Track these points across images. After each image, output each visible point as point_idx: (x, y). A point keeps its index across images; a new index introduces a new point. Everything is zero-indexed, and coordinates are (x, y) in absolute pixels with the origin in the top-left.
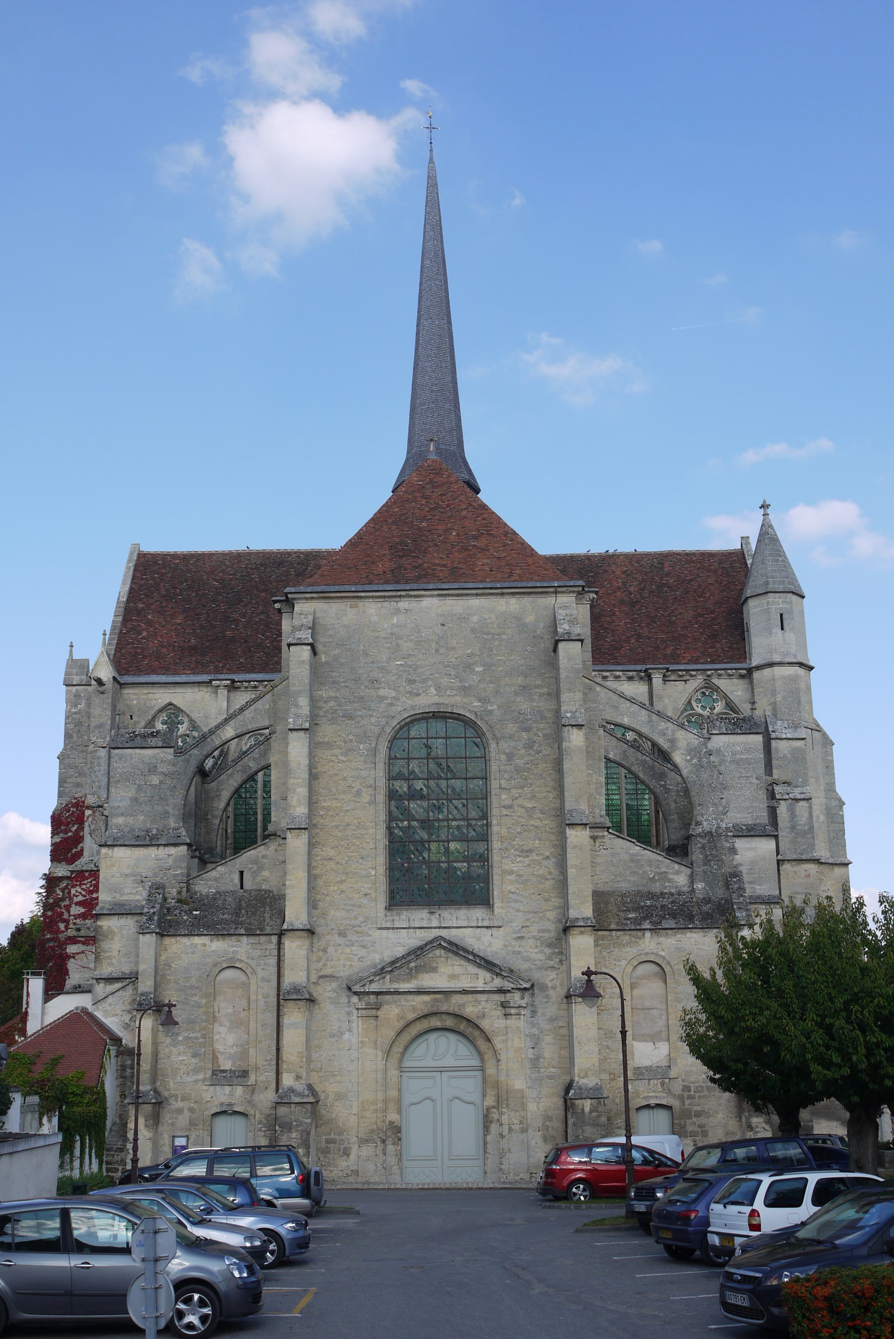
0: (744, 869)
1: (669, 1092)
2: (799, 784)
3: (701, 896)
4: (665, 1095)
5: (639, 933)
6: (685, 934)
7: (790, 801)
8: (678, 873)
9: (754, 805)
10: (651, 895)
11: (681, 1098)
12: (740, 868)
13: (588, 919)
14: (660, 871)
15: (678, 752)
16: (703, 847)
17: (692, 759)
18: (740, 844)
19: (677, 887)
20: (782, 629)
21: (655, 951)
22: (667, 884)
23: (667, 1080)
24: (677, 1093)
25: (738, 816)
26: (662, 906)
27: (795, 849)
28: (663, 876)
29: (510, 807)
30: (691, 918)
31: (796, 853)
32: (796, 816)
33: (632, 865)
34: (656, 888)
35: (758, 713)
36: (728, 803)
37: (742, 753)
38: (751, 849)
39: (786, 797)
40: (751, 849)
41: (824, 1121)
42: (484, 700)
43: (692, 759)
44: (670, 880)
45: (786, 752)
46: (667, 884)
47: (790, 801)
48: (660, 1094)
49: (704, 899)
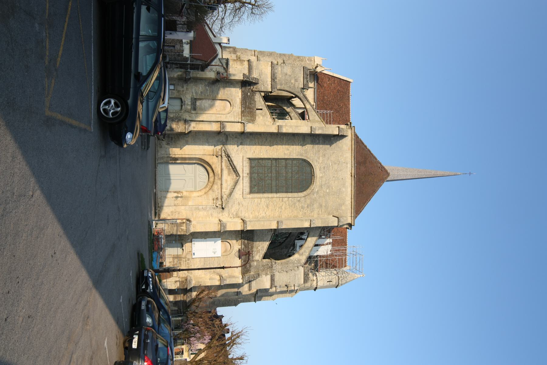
1: (187, 254)
4: (186, 252)
5: (240, 244)
18: (269, 277)
19: (255, 256)
21: (234, 249)
24: (187, 256)
28: (258, 251)
29: (282, 201)
38: (267, 280)
40: (267, 280)
42: (318, 192)
43: (296, 261)
44: (257, 254)
46: (256, 253)
49: (251, 265)
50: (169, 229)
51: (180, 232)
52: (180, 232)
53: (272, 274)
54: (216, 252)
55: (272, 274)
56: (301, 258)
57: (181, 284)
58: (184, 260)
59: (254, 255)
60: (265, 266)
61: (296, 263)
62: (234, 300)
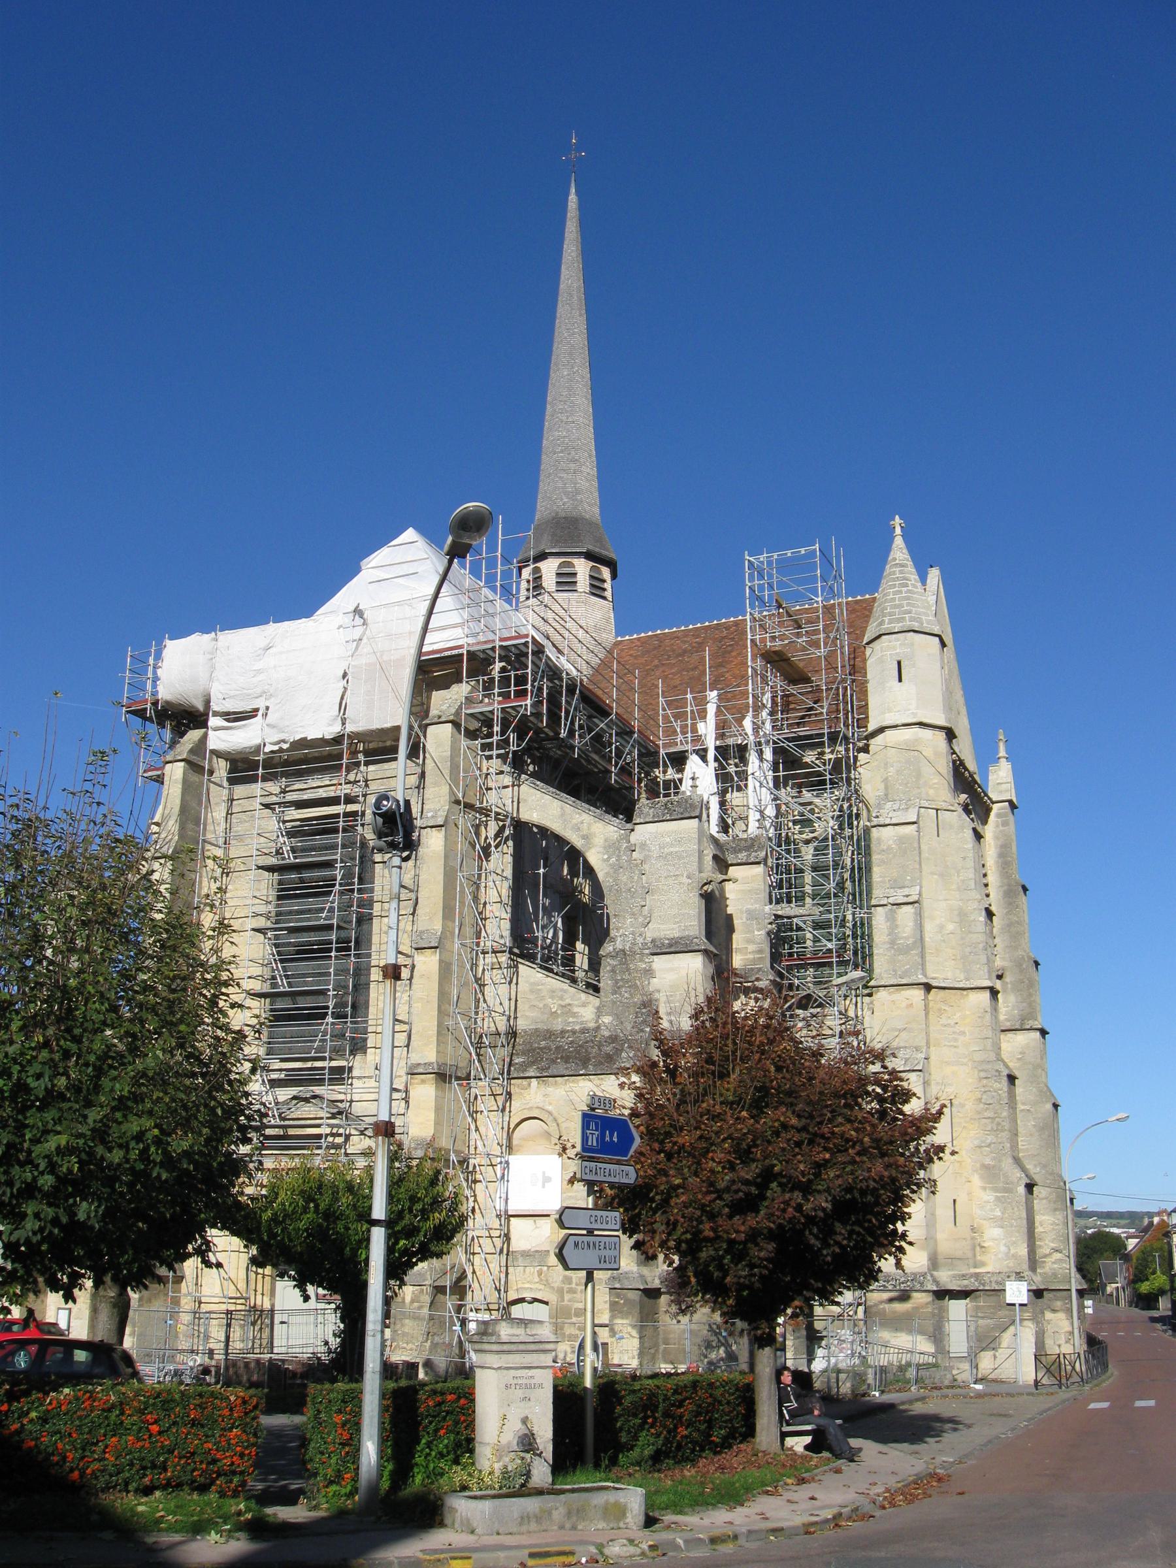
0: (662, 997)
1: (547, 1284)
2: (907, 883)
3: (607, 1034)
4: (542, 1287)
5: (525, 1082)
6: (577, 1082)
7: (889, 907)
8: (584, 1005)
9: (683, 911)
10: (550, 1035)
11: (560, 1292)
12: (656, 996)
13: (430, 1064)
14: (563, 1003)
15: (593, 851)
16: (613, 971)
17: (609, 858)
18: (659, 963)
19: (582, 1023)
20: (900, 680)
21: (540, 1105)
22: (571, 1020)
23: (545, 1268)
24: (556, 1285)
25: (664, 928)
26: (558, 1048)
27: (895, 971)
28: (567, 1010)
30: (585, 1062)
31: (895, 976)
32: (897, 926)
33: (532, 997)
34: (558, 1025)
35: (699, 791)
36: (651, 912)
37: (672, 845)
38: (672, 969)
39: (884, 902)
40: (672, 969)
41: (903, 1334)
43: (609, 858)
44: (574, 1015)
45: (891, 842)
46: (571, 1020)
47: (889, 907)
48: (537, 1286)
49: (610, 1037)
50: (410, 1346)
51: (420, 1308)
52: (420, 1308)
53: (647, 951)
54: (544, 1173)
55: (647, 951)
56: (599, 841)
57: (621, 1312)
58: (567, 1297)
59: (577, 1028)
60: (617, 982)
61: (619, 858)
62: (981, 1079)
